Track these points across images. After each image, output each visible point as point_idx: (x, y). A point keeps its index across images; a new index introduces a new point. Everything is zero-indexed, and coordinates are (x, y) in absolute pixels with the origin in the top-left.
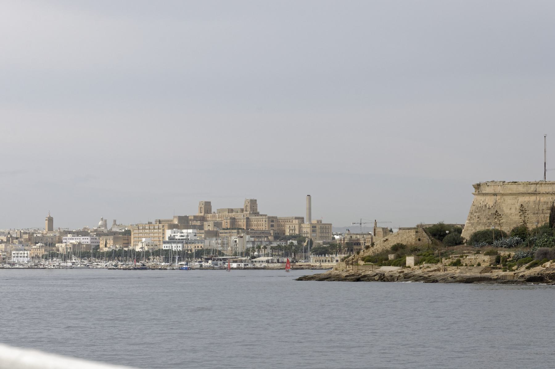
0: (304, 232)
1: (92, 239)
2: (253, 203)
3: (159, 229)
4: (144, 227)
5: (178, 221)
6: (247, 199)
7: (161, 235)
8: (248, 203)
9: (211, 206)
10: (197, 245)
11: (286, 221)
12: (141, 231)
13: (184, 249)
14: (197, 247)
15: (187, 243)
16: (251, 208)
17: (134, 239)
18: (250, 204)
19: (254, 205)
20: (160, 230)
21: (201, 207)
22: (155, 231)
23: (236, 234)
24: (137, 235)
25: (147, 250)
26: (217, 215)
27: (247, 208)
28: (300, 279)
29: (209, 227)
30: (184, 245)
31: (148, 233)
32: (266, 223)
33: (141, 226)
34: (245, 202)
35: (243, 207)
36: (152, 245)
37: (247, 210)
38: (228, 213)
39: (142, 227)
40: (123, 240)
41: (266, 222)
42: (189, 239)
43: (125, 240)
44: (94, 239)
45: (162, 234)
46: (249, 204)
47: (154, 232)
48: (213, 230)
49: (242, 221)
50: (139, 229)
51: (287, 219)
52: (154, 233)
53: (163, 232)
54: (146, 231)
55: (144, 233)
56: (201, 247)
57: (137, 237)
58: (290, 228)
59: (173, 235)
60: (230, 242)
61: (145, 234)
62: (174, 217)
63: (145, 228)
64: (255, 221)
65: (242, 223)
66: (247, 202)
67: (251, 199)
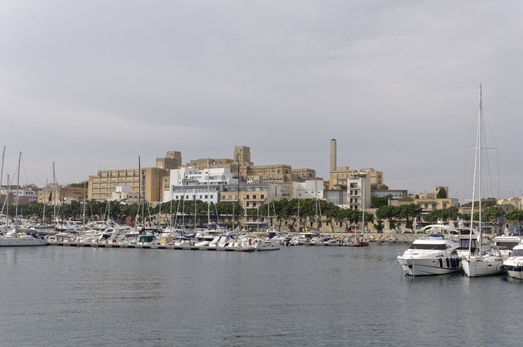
1: (27, 193)
2: (246, 150)
3: (134, 176)
4: (110, 174)
5: (164, 166)
6: (237, 146)
9: (181, 158)
12: (105, 180)
13: (221, 201)
14: (251, 197)
15: (225, 190)
17: (92, 191)
18: (244, 152)
19: (247, 154)
22: (128, 179)
23: (282, 181)
24: (97, 186)
30: (222, 194)
31: (117, 182)
33: (105, 172)
34: (235, 150)
39: (106, 175)
40: (74, 193)
41: (279, 172)
43: (76, 193)
44: (29, 193)
46: (242, 152)
47: (127, 181)
50: (101, 177)
52: (126, 182)
54: (113, 179)
57: (98, 189)
58: (338, 178)
59: (189, 176)
61: (111, 183)
62: (158, 160)
63: (111, 176)
64: (259, 172)
66: (238, 150)
67: (245, 146)
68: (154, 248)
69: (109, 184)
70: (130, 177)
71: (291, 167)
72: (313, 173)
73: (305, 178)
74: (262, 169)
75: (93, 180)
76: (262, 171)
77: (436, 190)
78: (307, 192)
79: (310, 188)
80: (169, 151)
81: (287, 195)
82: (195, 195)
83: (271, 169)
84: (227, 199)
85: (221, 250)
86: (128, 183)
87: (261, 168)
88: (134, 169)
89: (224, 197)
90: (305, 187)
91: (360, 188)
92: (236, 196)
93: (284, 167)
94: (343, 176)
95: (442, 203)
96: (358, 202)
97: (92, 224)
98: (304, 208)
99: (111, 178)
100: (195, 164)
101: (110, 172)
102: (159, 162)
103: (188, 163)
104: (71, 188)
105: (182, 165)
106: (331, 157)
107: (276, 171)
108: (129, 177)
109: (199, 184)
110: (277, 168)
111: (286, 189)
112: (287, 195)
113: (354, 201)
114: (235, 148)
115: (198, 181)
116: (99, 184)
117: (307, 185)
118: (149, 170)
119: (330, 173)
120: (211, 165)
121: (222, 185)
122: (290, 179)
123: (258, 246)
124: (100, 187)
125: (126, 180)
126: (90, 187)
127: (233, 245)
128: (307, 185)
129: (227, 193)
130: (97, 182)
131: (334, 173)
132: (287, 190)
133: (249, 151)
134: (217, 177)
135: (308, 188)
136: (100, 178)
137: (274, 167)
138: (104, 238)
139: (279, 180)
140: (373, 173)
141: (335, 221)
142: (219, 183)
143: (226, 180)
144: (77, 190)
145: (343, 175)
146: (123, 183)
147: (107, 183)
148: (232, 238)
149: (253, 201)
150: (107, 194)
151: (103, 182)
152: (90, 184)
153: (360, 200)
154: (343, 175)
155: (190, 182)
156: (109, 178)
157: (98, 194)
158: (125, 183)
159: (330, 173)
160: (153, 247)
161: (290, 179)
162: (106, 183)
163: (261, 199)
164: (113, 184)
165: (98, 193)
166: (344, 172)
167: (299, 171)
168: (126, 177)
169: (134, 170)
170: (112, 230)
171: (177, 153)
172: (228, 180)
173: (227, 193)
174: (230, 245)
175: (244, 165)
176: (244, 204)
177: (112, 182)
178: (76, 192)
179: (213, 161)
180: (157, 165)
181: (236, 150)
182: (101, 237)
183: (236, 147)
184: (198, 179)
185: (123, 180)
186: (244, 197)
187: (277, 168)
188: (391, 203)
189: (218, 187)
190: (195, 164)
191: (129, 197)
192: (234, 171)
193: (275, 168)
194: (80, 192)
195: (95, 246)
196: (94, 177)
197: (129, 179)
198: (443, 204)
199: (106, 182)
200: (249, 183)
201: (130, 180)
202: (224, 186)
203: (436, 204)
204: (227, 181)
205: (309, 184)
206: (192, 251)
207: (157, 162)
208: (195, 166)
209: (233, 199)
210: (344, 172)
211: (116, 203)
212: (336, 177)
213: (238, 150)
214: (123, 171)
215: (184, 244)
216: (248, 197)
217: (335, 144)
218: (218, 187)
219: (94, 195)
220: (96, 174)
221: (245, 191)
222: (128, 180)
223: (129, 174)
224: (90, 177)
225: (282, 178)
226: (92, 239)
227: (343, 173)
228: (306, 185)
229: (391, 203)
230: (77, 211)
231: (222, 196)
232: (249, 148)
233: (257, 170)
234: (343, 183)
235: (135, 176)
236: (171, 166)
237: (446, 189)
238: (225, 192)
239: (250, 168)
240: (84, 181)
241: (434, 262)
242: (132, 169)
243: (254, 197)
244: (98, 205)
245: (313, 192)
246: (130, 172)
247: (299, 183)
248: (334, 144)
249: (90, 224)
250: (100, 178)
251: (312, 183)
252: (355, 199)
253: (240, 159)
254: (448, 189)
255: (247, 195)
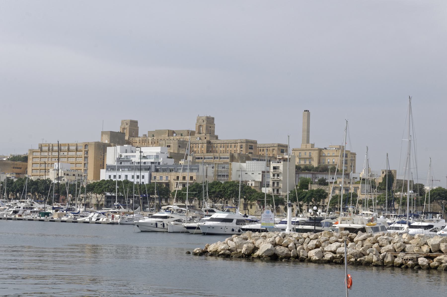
0: (329, 163)
2: (210, 121)
3: (77, 150)
4: (51, 148)
5: (109, 140)
6: (200, 116)
7: (82, 160)
8: (203, 122)
9: (138, 127)
10: (181, 174)
11: (260, 150)
12: (46, 154)
13: (152, 181)
14: (181, 178)
15: (157, 170)
16: (207, 129)
17: (32, 166)
20: (78, 153)
21: (124, 128)
22: (70, 153)
24: (38, 160)
25: (317, 166)
26: (150, 139)
27: (201, 128)
28: (174, 218)
29: (169, 148)
30: (154, 174)
32: (241, 149)
33: (46, 146)
35: (193, 128)
36: (74, 175)
37: (201, 132)
38: (168, 136)
39: (47, 148)
40: (13, 168)
41: (241, 148)
42: (159, 163)
45: (83, 158)
46: (205, 123)
47: (69, 156)
48: (176, 152)
49: (200, 147)
50: (41, 151)
51: (263, 147)
52: (68, 158)
53: (86, 156)
55: (50, 157)
56: (191, 178)
57: (39, 164)
59: (124, 155)
60: (277, 170)
61: (52, 158)
62: (103, 133)
63: (52, 150)
65: (199, 149)
66: (201, 121)
68: (46, 221)
69: (50, 159)
70: (72, 151)
71: (256, 142)
72: (286, 149)
73: (254, 156)
74: (224, 144)
75: (33, 154)
76: (224, 146)
77: (382, 173)
78: (247, 174)
79: (251, 169)
80: (124, 120)
81: (226, 177)
82: (133, 175)
83: (234, 144)
84: (158, 180)
85: (93, 223)
86: (70, 159)
87: (223, 142)
88: (76, 142)
89: (155, 177)
90: (245, 168)
91: (282, 172)
92: (167, 176)
93: (247, 142)
94: (305, 155)
95: (353, 188)
96: (280, 186)
97: (15, 202)
98: (221, 191)
99: (52, 152)
100: (153, 135)
101: (51, 145)
102: (104, 135)
103: (145, 135)
104: (9, 161)
105: (139, 136)
106: (303, 131)
107: (238, 146)
108: (71, 151)
109: (133, 163)
110: (239, 143)
111: (224, 170)
112: (226, 177)
113: (276, 185)
114: (197, 118)
115: (132, 160)
116: (39, 159)
117: (247, 166)
118: (92, 144)
119: (292, 150)
120: (170, 137)
121: (153, 165)
122: (237, 158)
123: (121, 221)
124: (41, 162)
125: (68, 155)
126: (30, 162)
127: (103, 219)
128: (247, 166)
129: (158, 174)
130: (37, 157)
131: (296, 151)
132: (226, 171)
133: (213, 122)
134: (151, 157)
135: (249, 169)
136: (41, 152)
137: (237, 142)
138: (14, 213)
139: (225, 159)
140: (338, 152)
141: (258, 204)
142: (152, 163)
143: (159, 160)
144: (16, 165)
145: (305, 153)
146: (65, 159)
147: (48, 158)
148: (104, 215)
149: (182, 183)
150: (48, 170)
151: (44, 157)
152: (30, 158)
153: (281, 184)
154: (305, 153)
155: (124, 161)
156: (50, 153)
157: (38, 169)
158: (67, 159)
159: (292, 150)
160: (46, 220)
161: (237, 158)
162: (47, 158)
163: (190, 180)
164: (55, 159)
165: (38, 168)
166: (306, 150)
167: (269, 146)
168: (68, 152)
169: (77, 144)
170: (20, 207)
171: (133, 122)
172: (161, 160)
173: (158, 174)
174: (101, 220)
175: (204, 138)
176: (174, 185)
177: (53, 157)
178: (16, 166)
179: (174, 132)
180: (102, 139)
181: (198, 120)
182: (11, 213)
183: (199, 117)
184: (132, 159)
185: (64, 155)
186: (174, 178)
187: (239, 143)
188: (311, 188)
189: (150, 167)
190: (153, 136)
191: (66, 174)
192: (182, 148)
193: (237, 143)
194: (20, 166)
195: (5, 219)
196: (34, 151)
197: (71, 154)
198: (354, 189)
199: (47, 157)
200: (181, 164)
201: (72, 155)
202: (155, 166)
203: (348, 189)
204: (160, 161)
205: (250, 164)
206: (73, 223)
207: (102, 135)
208: (152, 138)
209: (164, 180)
210: (306, 150)
211: (48, 181)
212: (299, 155)
213: (200, 121)
214: (65, 145)
215: (70, 219)
216: (178, 178)
217: (308, 116)
218: (150, 167)
219: (33, 171)
220: (37, 148)
221: (176, 172)
222: (70, 155)
223: (71, 148)
224: (30, 150)
225: (229, 156)
226: (4, 214)
227: (306, 151)
228: (247, 165)
229: (311, 188)
230: (10, 189)
231: (153, 176)
232: (213, 119)
233: (218, 145)
234: (305, 162)
235: (78, 151)
236: (117, 140)
237: (393, 172)
238: (156, 173)
239: (211, 142)
240: (26, 154)
241: (152, 224)
242: (74, 142)
243: (184, 178)
244: (30, 183)
245: (253, 174)
246: (72, 146)
247: (241, 163)
248: (307, 115)
249: (13, 202)
250: (41, 152)
251: (253, 164)
252: (277, 182)
253: (203, 131)
254: (396, 172)
255: (177, 177)
